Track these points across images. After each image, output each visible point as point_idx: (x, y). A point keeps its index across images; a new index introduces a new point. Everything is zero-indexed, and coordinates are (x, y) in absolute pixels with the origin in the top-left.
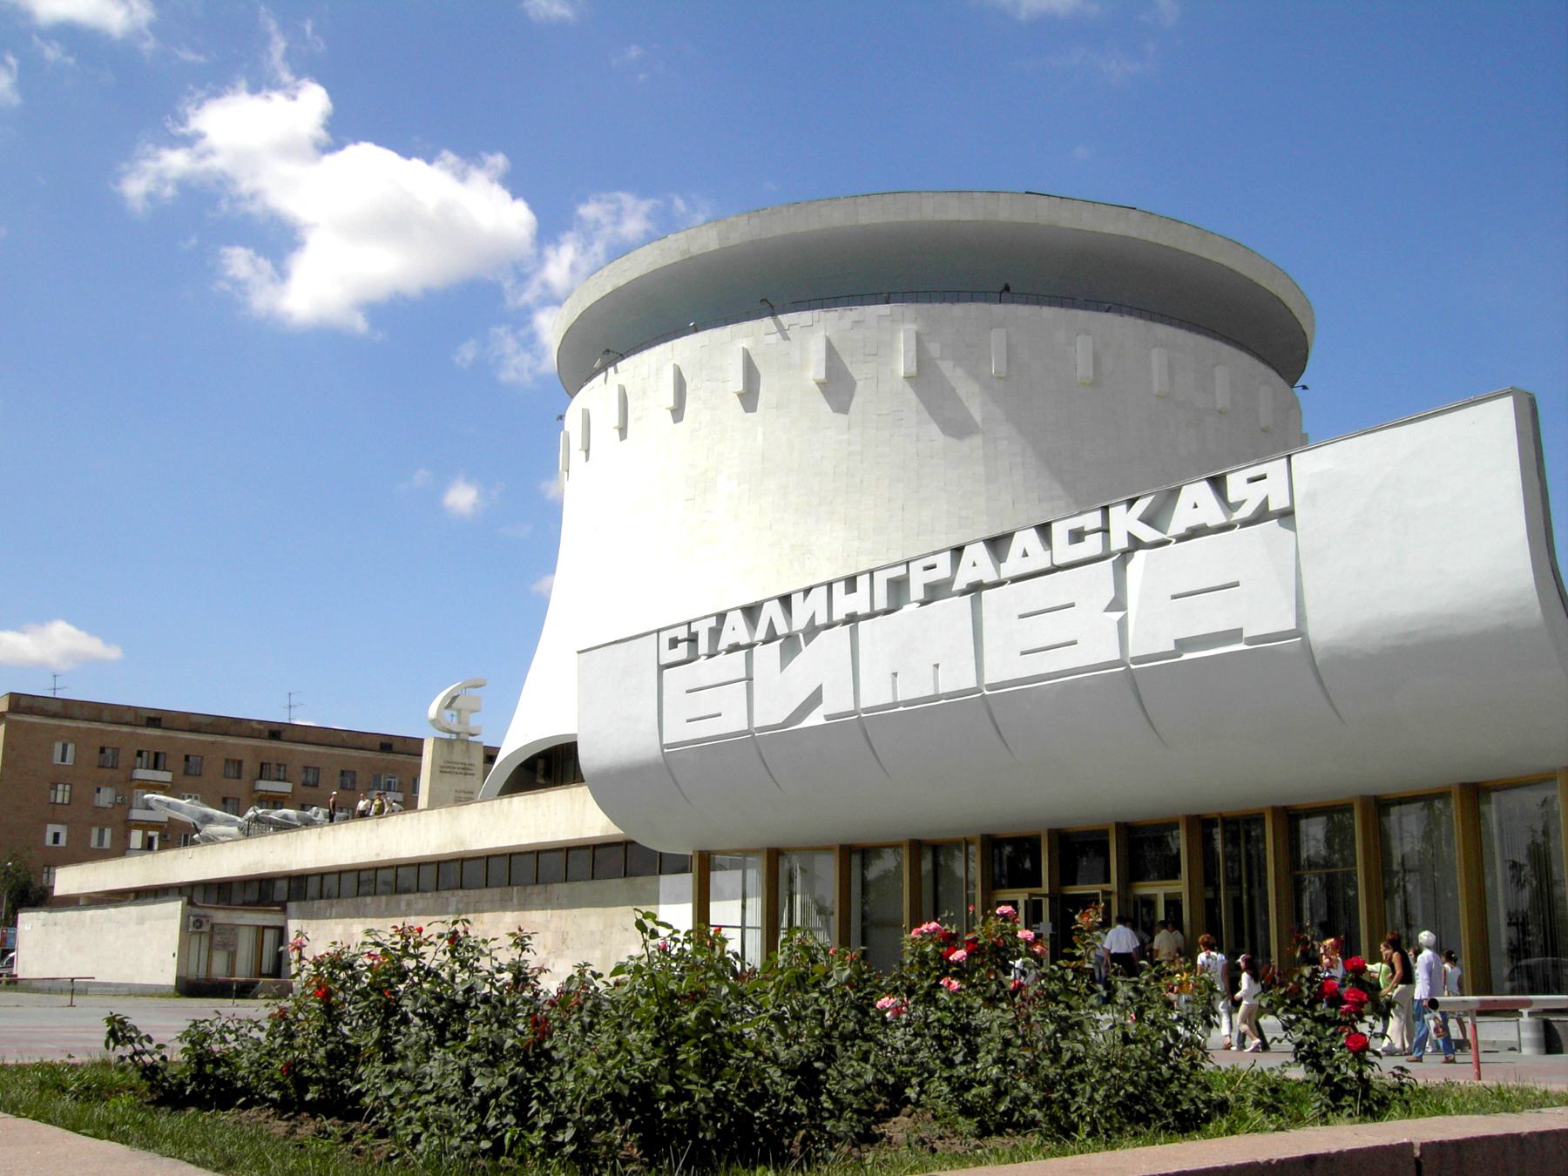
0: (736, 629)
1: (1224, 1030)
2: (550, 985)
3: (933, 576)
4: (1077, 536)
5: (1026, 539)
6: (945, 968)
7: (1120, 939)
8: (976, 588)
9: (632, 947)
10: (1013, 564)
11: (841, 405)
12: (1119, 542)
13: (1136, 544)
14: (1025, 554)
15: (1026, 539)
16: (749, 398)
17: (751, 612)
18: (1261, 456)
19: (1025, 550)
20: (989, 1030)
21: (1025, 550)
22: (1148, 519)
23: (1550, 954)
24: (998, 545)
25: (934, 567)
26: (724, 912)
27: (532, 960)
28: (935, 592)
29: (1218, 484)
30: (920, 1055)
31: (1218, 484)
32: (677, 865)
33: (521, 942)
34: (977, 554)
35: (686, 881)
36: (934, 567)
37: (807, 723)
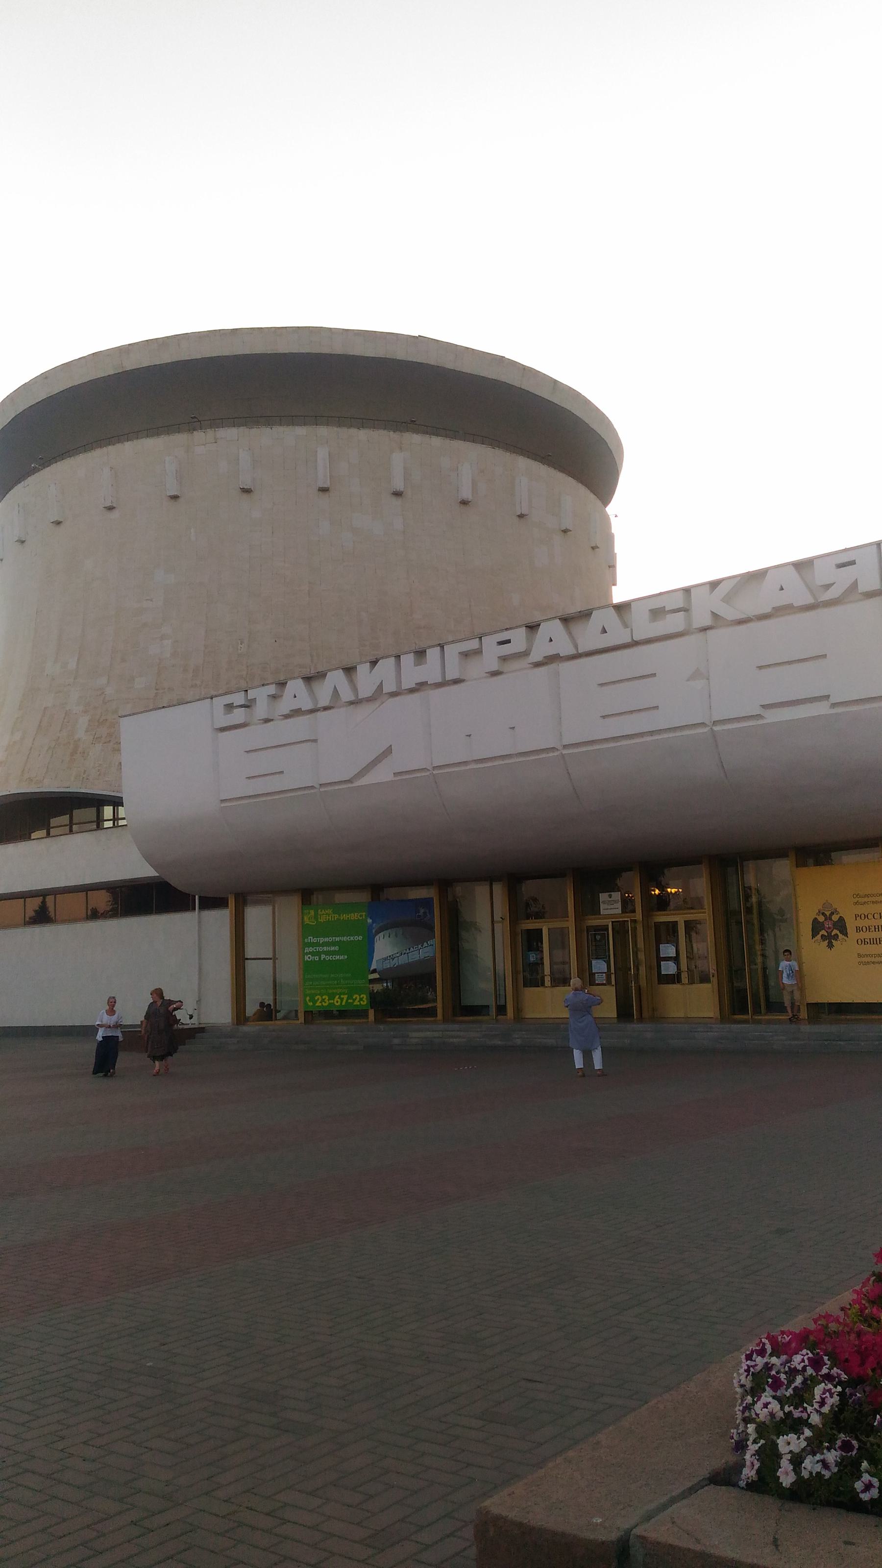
0: (389, 958)
1: (429, 994)
2: (375, 991)
3: (506, 649)
4: (416, 948)
5: (411, 948)
6: (406, 989)
7: (420, 986)
8: (408, 953)
9: (382, 988)
10: (411, 951)
11: (397, 937)
12: (419, 948)
13: (420, 948)
14: (604, 631)
15: (411, 948)
16: (389, 937)
17: (390, 956)
18: (430, 940)
19: (604, 628)
20: (759, 1418)
21: (604, 628)
22: (422, 946)
23: (763, 1010)
24: (409, 949)
25: (508, 641)
26: (389, 984)
27: (374, 989)
28: (404, 954)
29: (427, 943)
30: (621, 1507)
31: (427, 943)
32: (385, 980)
33: (373, 987)
34: (408, 950)
35: (385, 981)
36: (508, 641)
37: (366, 780)
